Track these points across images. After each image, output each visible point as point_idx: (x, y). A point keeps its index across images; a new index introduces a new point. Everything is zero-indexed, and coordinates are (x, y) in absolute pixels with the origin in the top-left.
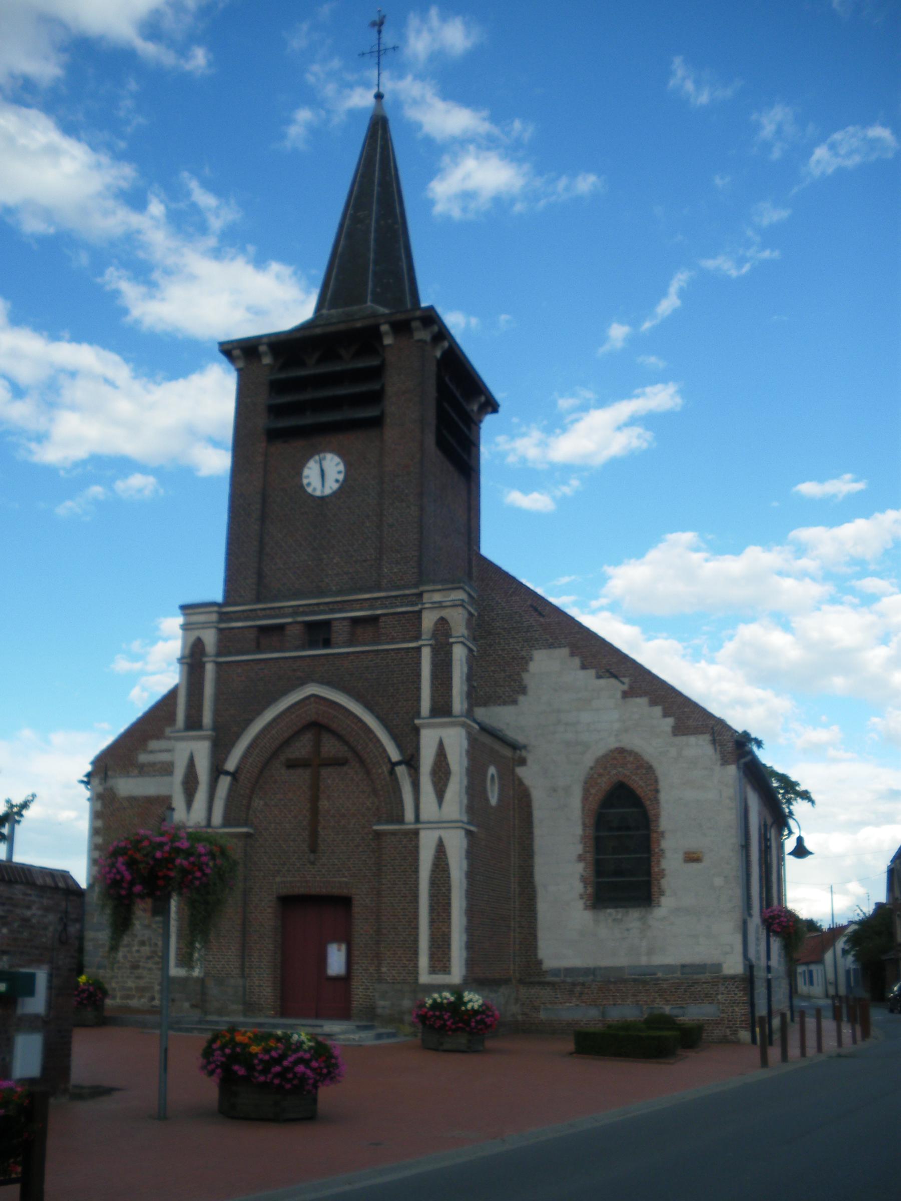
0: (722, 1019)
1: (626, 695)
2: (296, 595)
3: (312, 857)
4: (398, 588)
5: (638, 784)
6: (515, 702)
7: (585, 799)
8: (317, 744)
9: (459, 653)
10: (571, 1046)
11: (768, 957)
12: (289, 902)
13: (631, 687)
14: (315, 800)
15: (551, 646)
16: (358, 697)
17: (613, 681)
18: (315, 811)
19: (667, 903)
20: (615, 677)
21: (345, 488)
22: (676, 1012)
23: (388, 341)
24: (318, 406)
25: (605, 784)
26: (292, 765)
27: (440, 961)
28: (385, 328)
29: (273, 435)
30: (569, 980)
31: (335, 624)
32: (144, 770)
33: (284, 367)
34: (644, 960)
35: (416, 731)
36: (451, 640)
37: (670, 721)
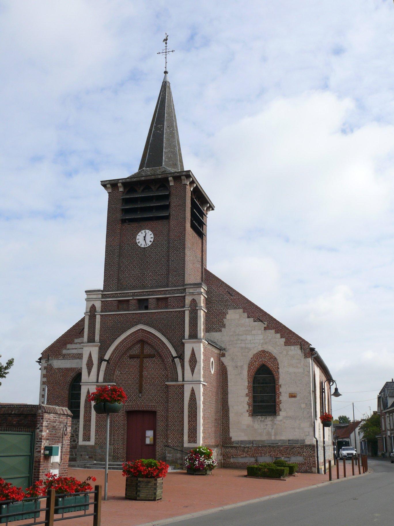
0: (305, 463)
1: (265, 329)
4: (175, 286)
5: (270, 365)
7: (249, 371)
9: (202, 314)
10: (245, 473)
11: (324, 438)
12: (130, 413)
13: (268, 326)
14: (141, 372)
16: (160, 330)
17: (260, 323)
18: (141, 376)
19: (282, 414)
20: (262, 321)
21: (154, 244)
22: (286, 459)
23: (172, 184)
24: (143, 210)
25: (257, 365)
26: (132, 357)
27: (87, 438)
29: (123, 221)
30: (243, 446)
32: (64, 357)
33: (128, 192)
34: (273, 438)
35: (183, 344)
36: (197, 308)
37: (284, 340)
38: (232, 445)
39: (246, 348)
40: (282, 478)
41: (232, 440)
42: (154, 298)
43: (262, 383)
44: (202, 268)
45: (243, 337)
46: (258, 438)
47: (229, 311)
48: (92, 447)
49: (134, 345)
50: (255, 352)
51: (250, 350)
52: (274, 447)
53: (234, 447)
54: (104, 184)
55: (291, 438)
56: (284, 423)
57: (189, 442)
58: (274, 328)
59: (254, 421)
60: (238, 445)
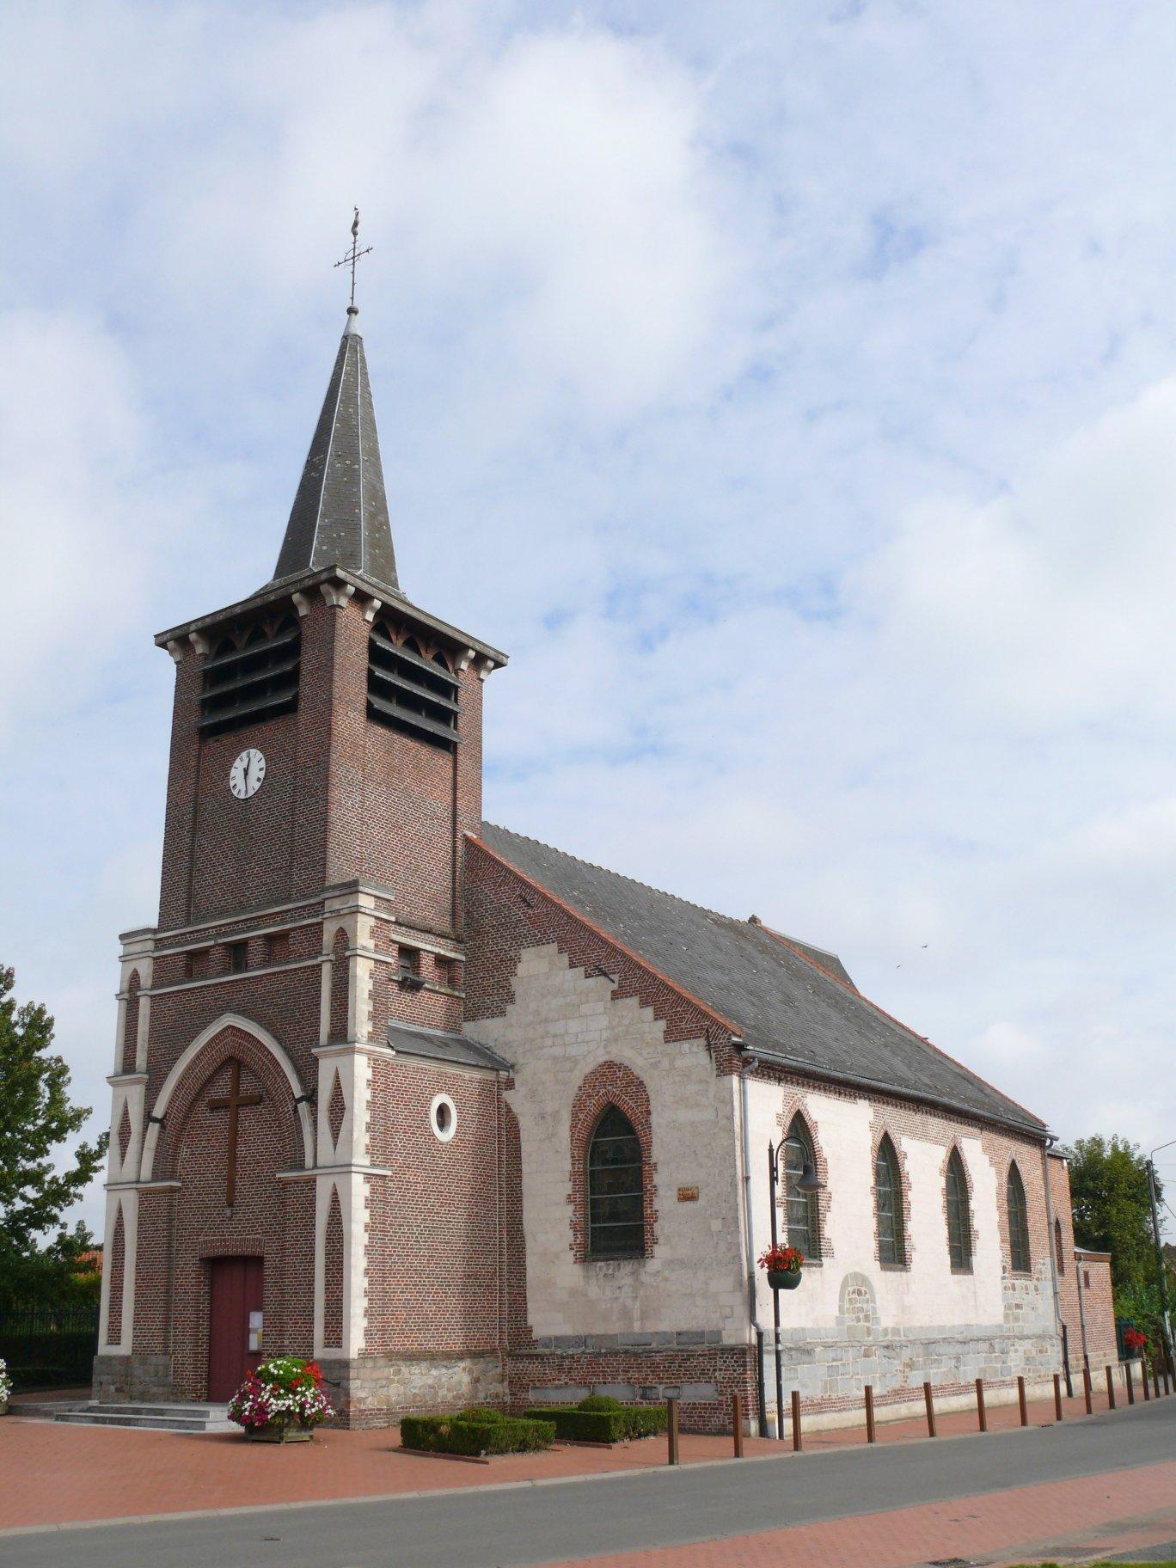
1: (615, 995)
2: (222, 913)
3: (228, 1212)
4: (305, 897)
5: (628, 1105)
6: (503, 1013)
7: (573, 1127)
8: (236, 1080)
13: (620, 986)
15: (539, 943)
17: (602, 979)
18: (233, 1159)
19: (661, 1252)
20: (605, 974)
23: (303, 611)
25: (593, 1106)
26: (214, 1106)
27: (115, 1339)
28: (296, 597)
30: (559, 1352)
31: (252, 943)
33: (220, 653)
37: (662, 1024)
38: (533, 1351)
39: (568, 1059)
40: (482, 1457)
41: (536, 1335)
42: (259, 937)
43: (614, 1161)
44: (454, 836)
45: (557, 1028)
46: (599, 1329)
47: (523, 952)
48: (126, 1360)
49: (217, 1071)
50: (588, 1070)
51: (576, 1062)
52: (636, 1355)
53: (537, 1356)
54: (162, 641)
55: (684, 1326)
56: (666, 1279)
57: (110, 1343)
58: (636, 992)
59: (587, 1278)
60: (547, 1351)
